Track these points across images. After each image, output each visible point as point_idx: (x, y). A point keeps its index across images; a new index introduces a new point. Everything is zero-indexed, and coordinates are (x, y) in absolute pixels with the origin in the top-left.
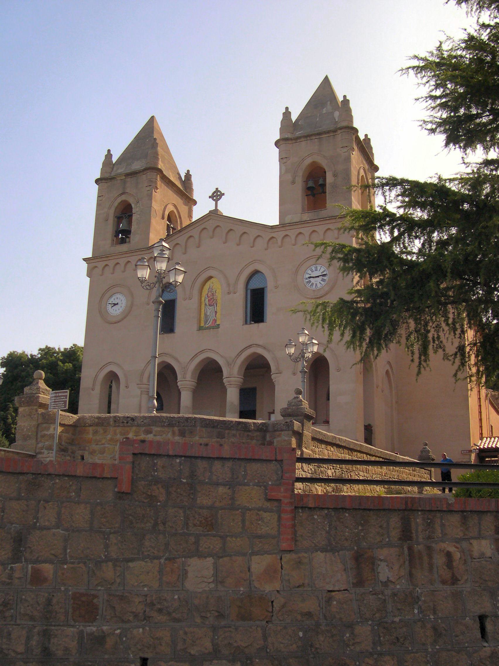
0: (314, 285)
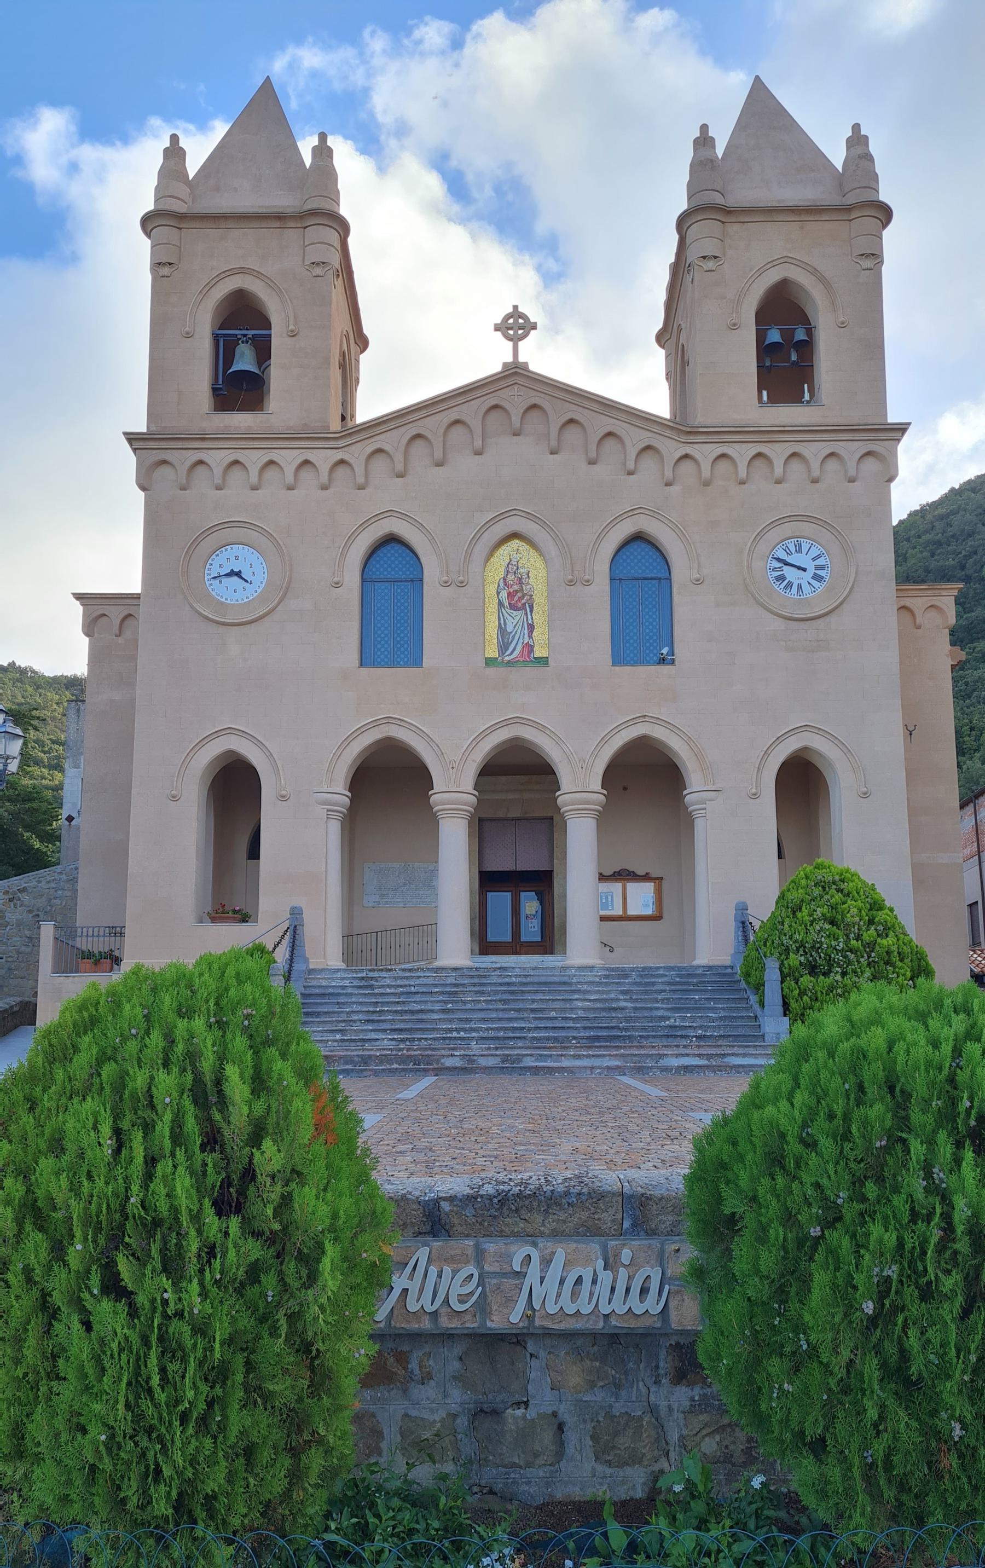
0: (795, 587)
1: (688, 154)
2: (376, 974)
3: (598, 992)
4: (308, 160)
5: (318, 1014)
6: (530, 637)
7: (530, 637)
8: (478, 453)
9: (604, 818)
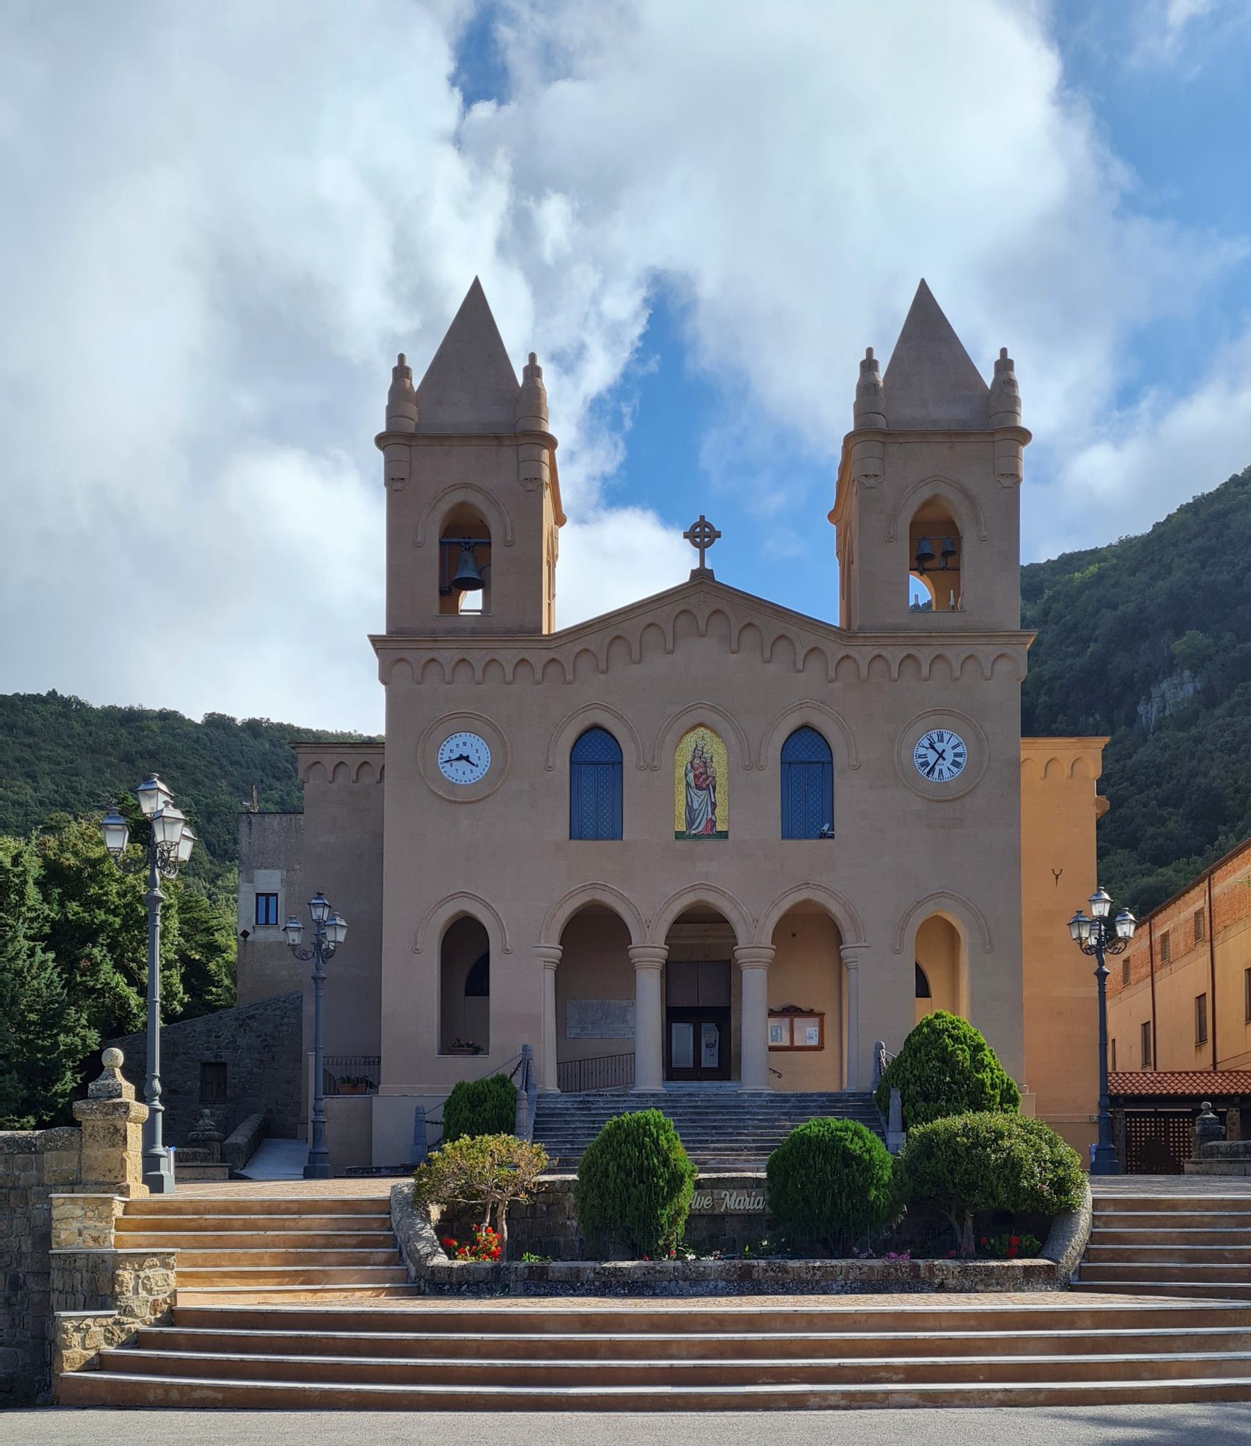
1: (855, 375)
2: (591, 1099)
3: (764, 1114)
4: (520, 381)
5: (551, 1129)
6: (713, 813)
7: (713, 813)
8: (671, 652)
9: (774, 968)
